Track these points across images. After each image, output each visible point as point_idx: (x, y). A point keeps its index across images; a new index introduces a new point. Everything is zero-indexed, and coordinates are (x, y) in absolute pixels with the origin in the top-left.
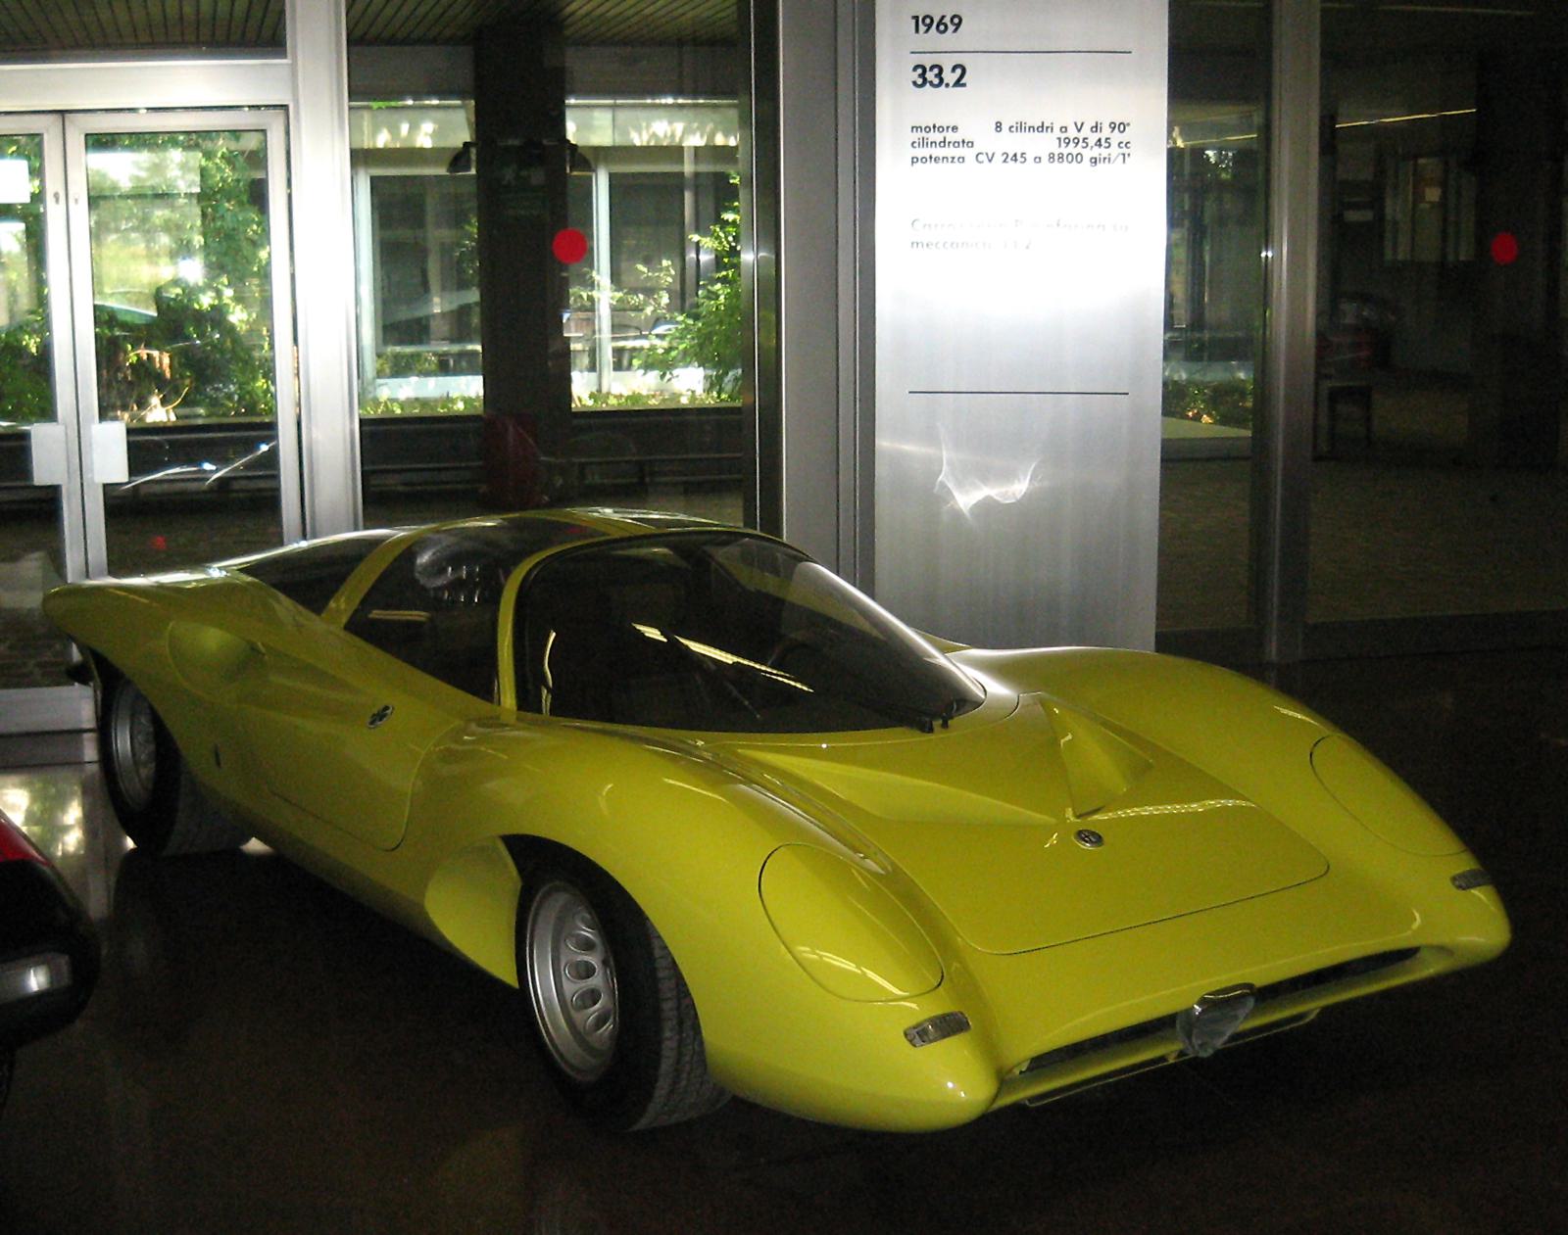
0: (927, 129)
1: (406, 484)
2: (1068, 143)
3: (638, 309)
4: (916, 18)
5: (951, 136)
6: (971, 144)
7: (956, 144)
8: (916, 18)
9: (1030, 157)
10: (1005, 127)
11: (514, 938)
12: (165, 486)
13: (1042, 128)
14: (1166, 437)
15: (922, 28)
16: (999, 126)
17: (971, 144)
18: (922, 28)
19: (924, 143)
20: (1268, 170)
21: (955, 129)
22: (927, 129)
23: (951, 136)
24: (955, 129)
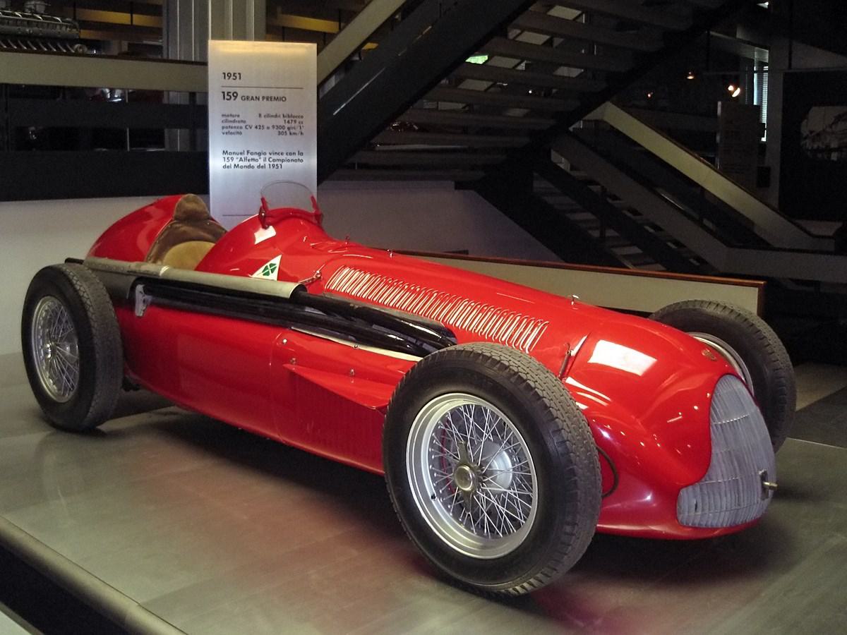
0: (228, 116)
1: (352, 320)
2: (230, 77)
3: (574, 428)
4: (224, 74)
5: (237, 119)
6: (244, 122)
7: (239, 122)
8: (224, 74)
9: (265, 127)
10: (263, 115)
11: (34, 201)
12: (518, 424)
13: (276, 116)
14: (206, 195)
15: (227, 77)
16: (260, 115)
17: (244, 122)
18: (227, 77)
19: (226, 121)
20: (364, 8)
21: (238, 116)
22: (228, 116)
23: (237, 119)
24: (238, 116)
